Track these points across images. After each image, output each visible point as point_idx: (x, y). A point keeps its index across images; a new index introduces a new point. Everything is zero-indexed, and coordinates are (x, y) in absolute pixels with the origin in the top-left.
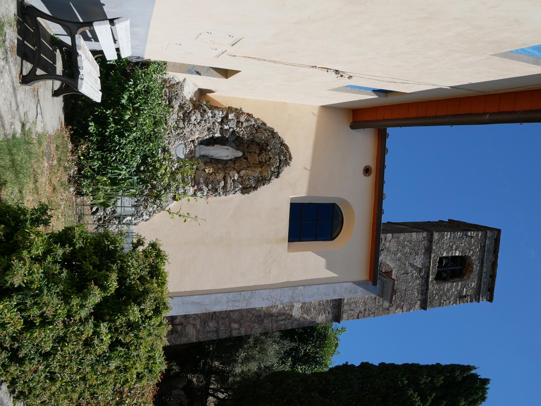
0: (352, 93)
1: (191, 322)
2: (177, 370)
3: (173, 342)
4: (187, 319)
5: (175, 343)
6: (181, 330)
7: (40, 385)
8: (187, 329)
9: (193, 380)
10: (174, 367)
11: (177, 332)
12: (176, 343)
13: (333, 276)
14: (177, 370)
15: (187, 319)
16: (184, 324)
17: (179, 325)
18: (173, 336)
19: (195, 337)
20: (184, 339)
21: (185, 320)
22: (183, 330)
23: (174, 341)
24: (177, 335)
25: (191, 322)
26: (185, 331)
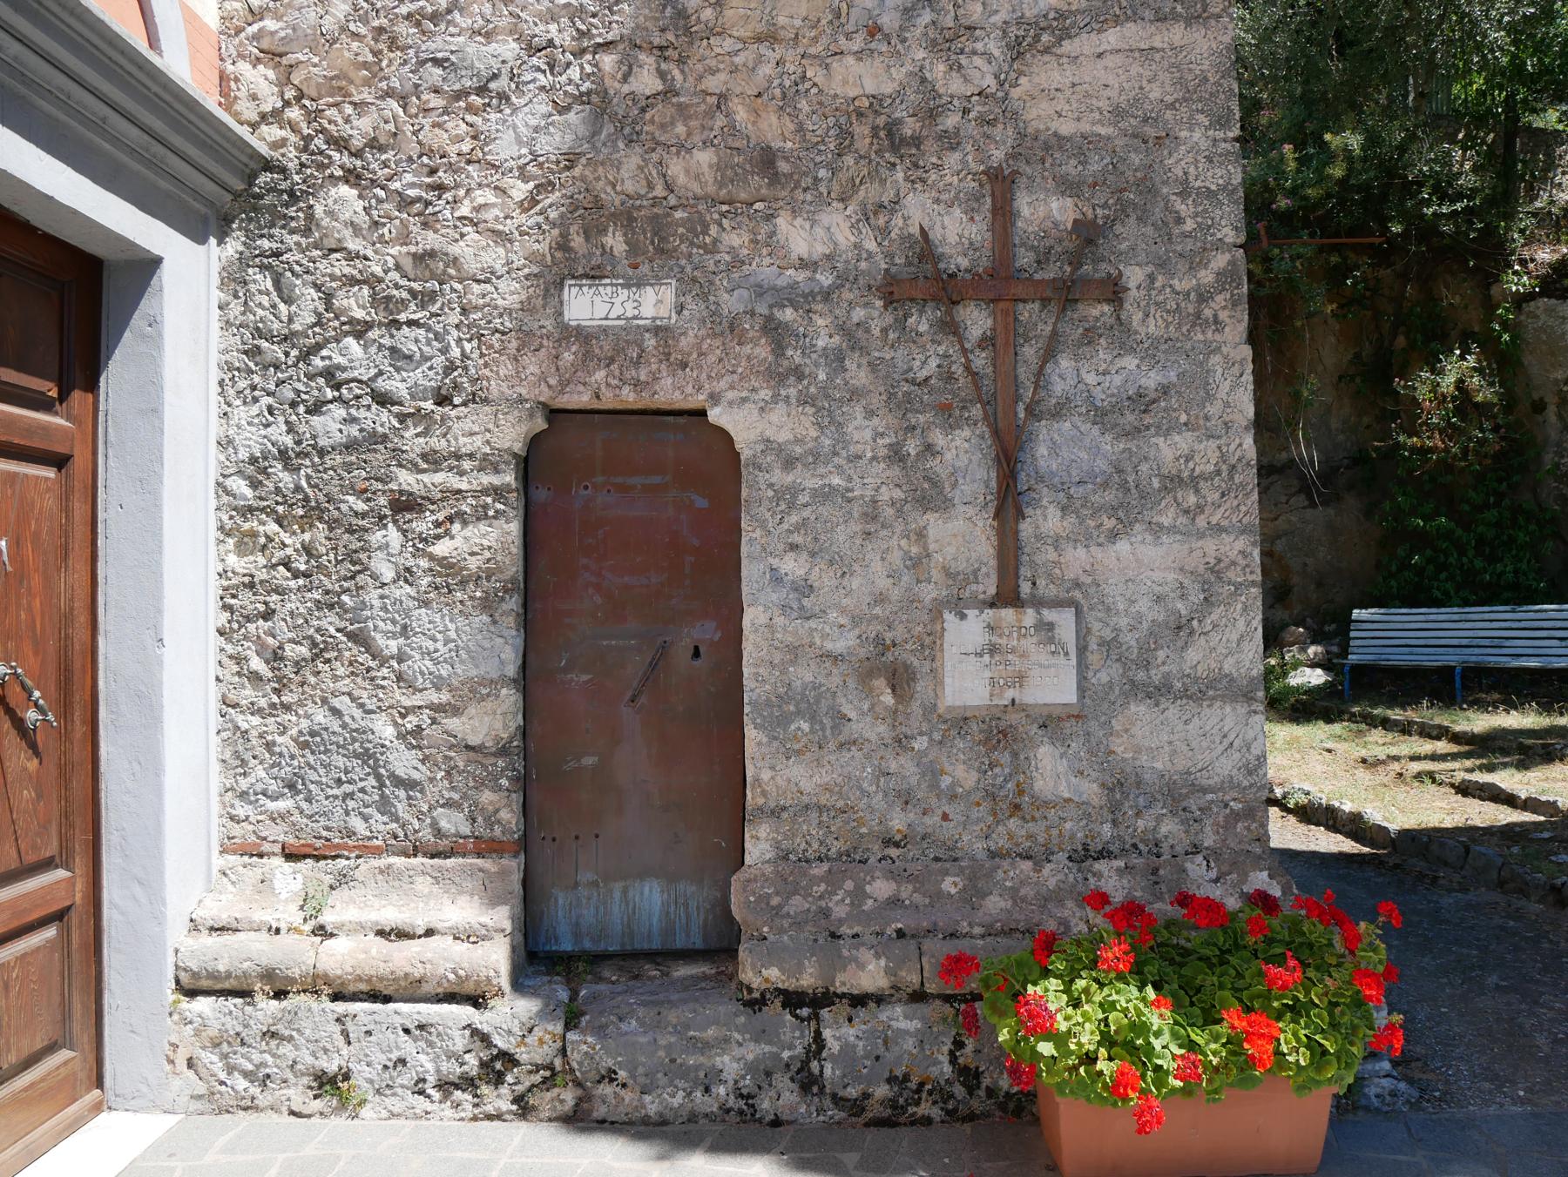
0: (158, 771)
1: (989, 82)
2: (1471, 360)
3: (1207, 276)
4: (951, 121)
5: (1220, 261)
6: (1068, 187)
7: (360, 523)
8: (1066, 128)
9: (1550, 265)
10: (1448, 382)
11: (1088, 235)
12: (1219, 245)
13: (1334, 849)
14: (1471, 360)
15: (951, 121)
16: (998, 155)
17: (1003, 214)
18: (1134, 276)
19: (1176, 33)
20: (1178, 162)
21: (951, 141)
22: (1071, 168)
23: (1195, 261)
24: (1129, 232)
25: (989, 82)
26: (1084, 145)
